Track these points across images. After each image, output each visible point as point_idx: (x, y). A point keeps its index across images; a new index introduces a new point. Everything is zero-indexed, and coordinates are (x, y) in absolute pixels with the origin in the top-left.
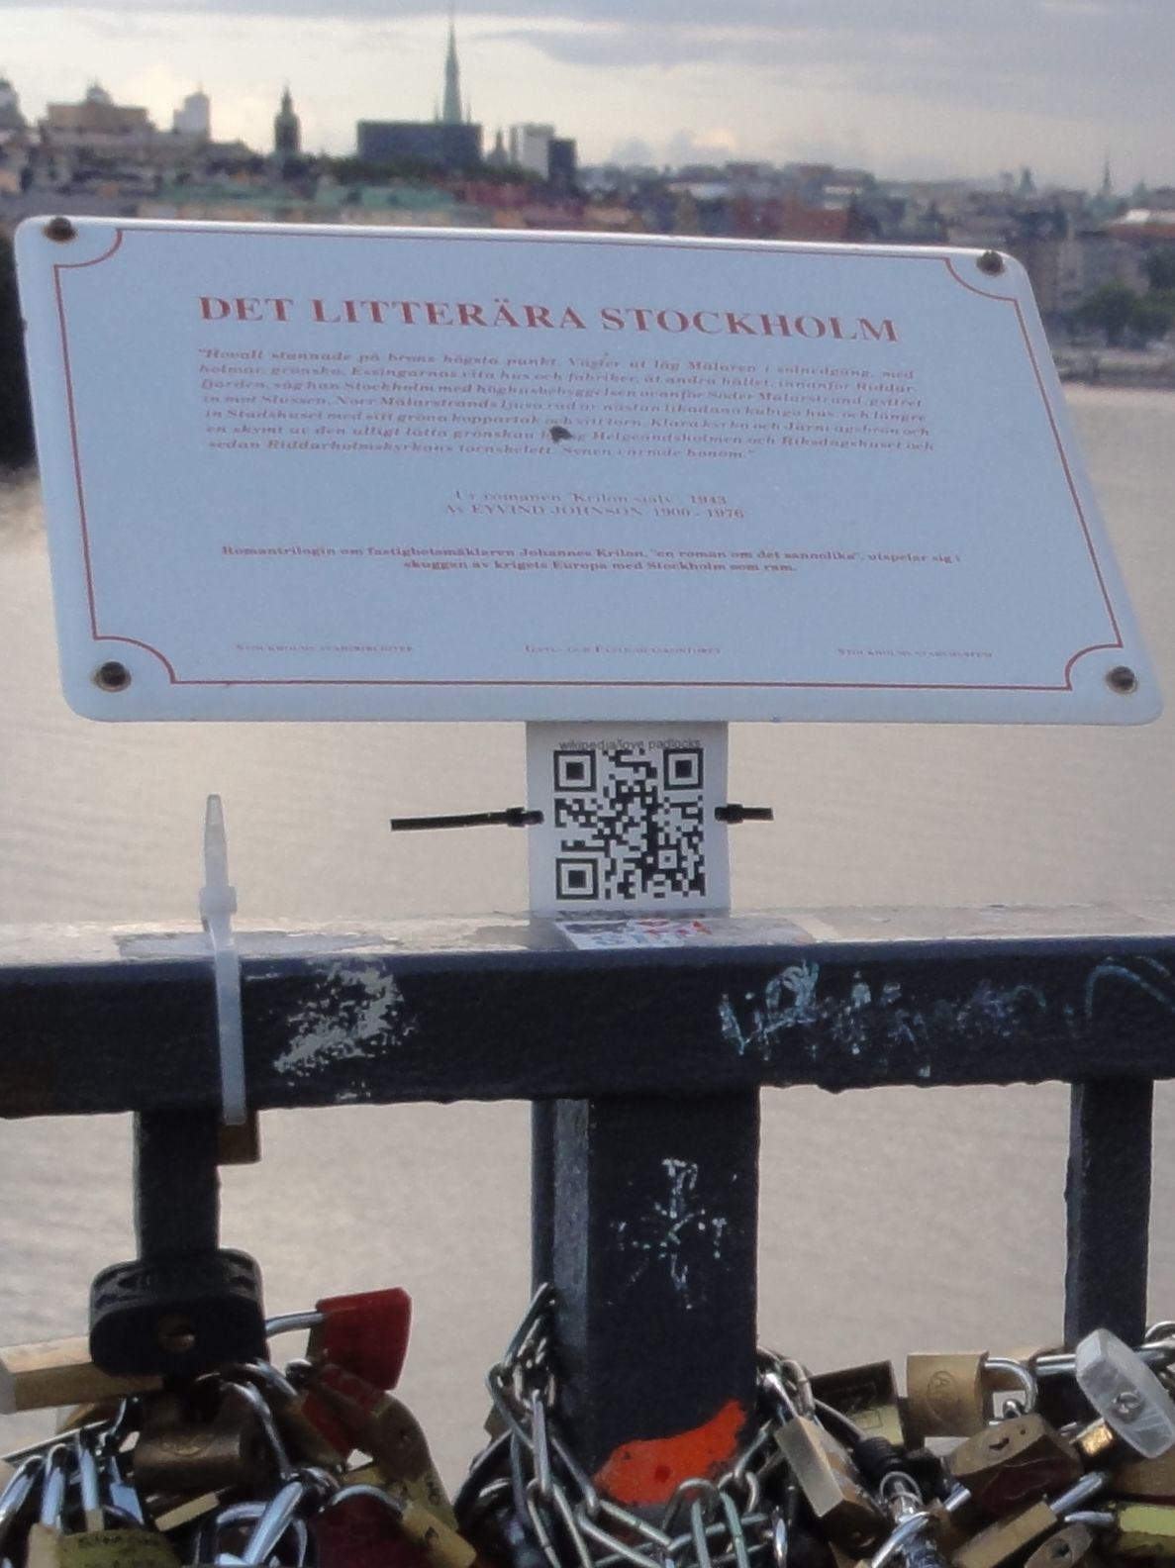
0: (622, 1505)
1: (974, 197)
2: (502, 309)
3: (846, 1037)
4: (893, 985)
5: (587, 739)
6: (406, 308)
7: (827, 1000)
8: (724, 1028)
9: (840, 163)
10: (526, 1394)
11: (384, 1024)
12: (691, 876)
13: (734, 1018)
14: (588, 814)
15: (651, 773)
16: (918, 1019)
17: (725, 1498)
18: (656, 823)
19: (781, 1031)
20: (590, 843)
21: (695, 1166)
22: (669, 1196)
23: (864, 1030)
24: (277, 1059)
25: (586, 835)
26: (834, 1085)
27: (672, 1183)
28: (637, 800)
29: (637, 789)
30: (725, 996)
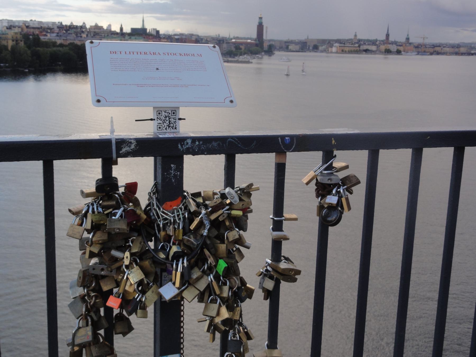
0: (166, 210)
1: (212, 38)
2: (150, 53)
5: (161, 109)
8: (179, 147)
9: (194, 33)
10: (153, 196)
11: (134, 147)
12: (175, 127)
14: (161, 119)
15: (169, 114)
16: (205, 146)
17: (179, 209)
19: (186, 148)
20: (161, 123)
25: (161, 122)
28: (168, 117)
29: (168, 116)
30: (179, 143)
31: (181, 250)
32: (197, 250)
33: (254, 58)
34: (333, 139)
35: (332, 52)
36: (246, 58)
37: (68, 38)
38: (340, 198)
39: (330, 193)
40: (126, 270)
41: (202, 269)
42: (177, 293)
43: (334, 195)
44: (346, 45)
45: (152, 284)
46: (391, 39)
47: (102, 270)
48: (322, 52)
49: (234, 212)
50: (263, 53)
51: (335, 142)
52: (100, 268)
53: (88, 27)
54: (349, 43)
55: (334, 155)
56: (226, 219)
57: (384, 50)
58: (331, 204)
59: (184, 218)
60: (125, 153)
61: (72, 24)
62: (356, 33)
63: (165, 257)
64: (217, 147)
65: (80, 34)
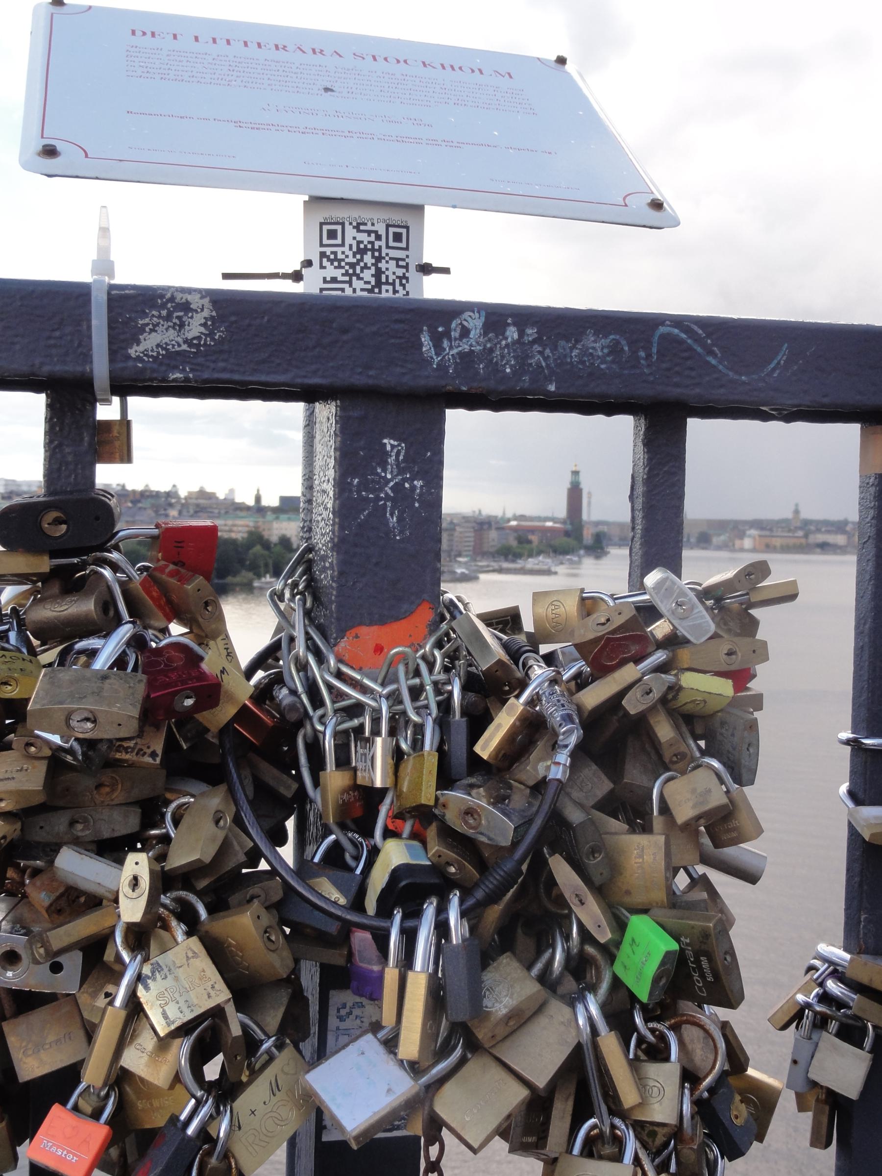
0: (352, 668)
3: (502, 361)
4: (532, 329)
7: (490, 335)
8: (424, 349)
11: (202, 329)
13: (430, 343)
15: (378, 237)
16: (548, 352)
18: (381, 268)
19: (459, 353)
20: (340, 278)
21: (403, 445)
22: (386, 463)
23: (513, 357)
24: (131, 348)
25: (338, 274)
27: (387, 454)
28: (369, 253)
29: (369, 246)
30: (425, 328)
31: (429, 863)
33: (562, 563)
35: (742, 550)
36: (543, 562)
37: (137, 518)
40: (126, 956)
42: (404, 1098)
44: (775, 534)
48: (719, 548)
50: (582, 552)
53: (183, 493)
54: (782, 528)
56: (652, 709)
59: (445, 706)
60: (155, 358)
61: (147, 488)
62: (797, 505)
64: (609, 359)
65: (165, 510)
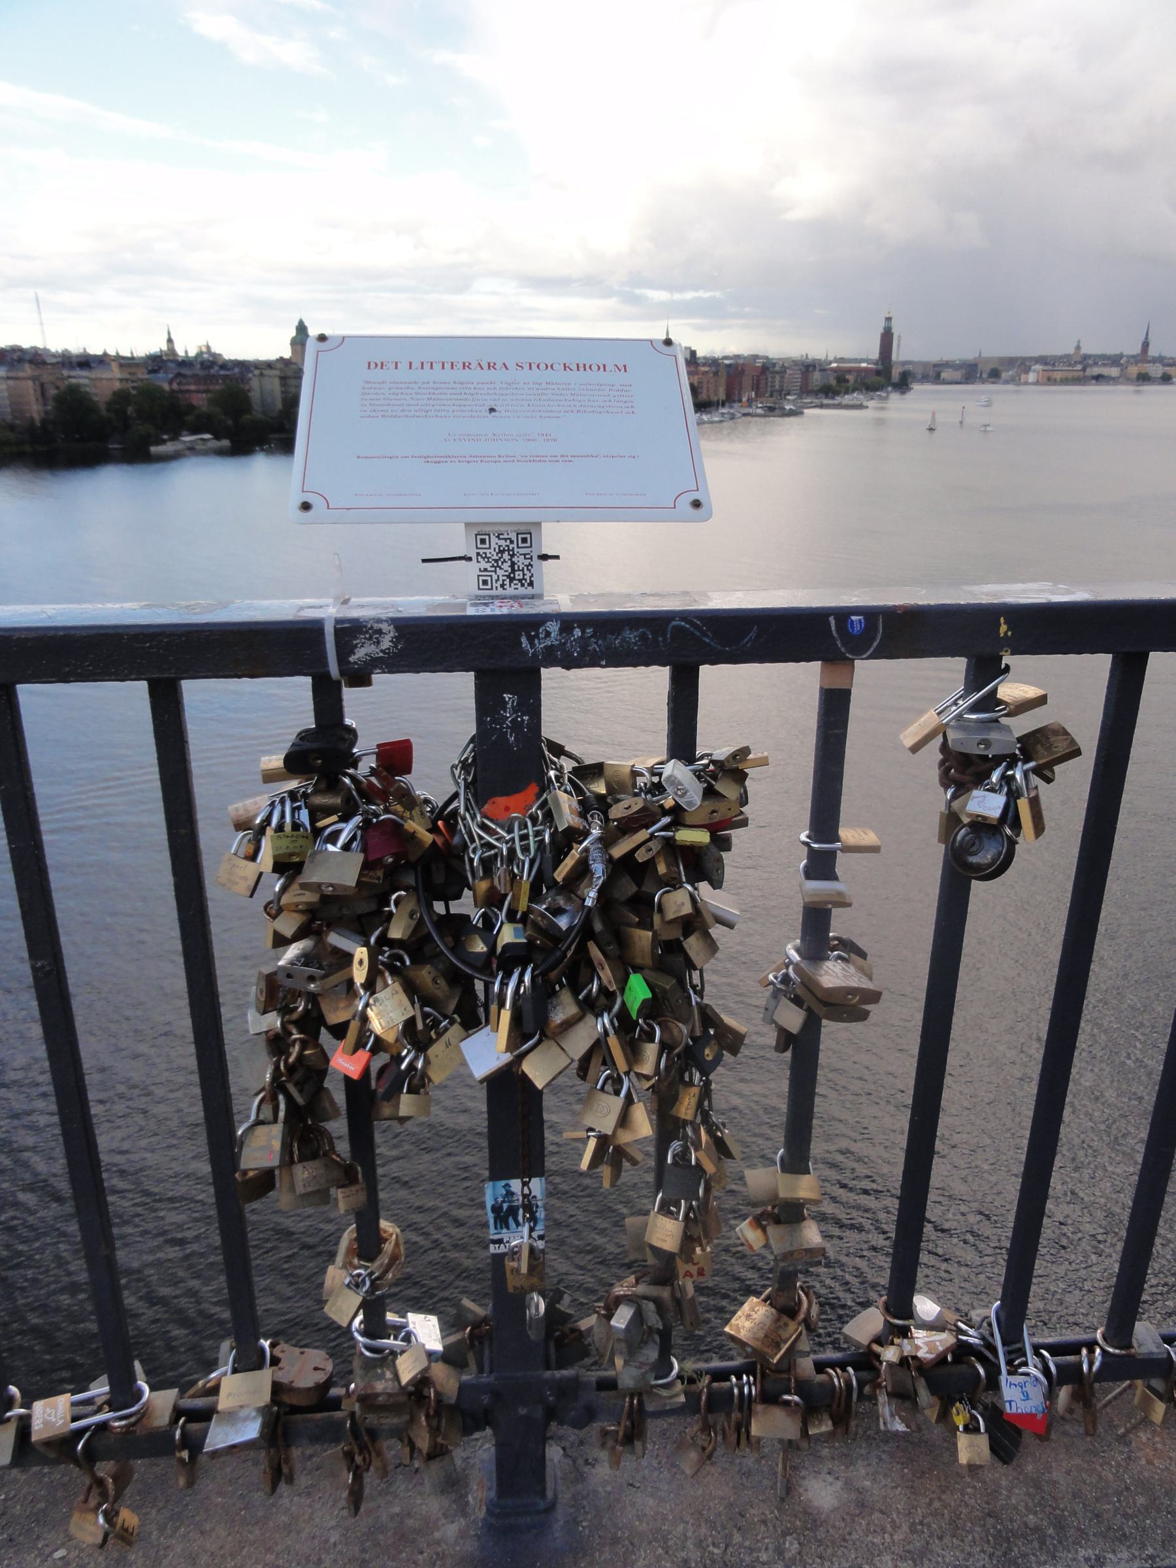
1: (793, 361)
5: (487, 529)
6: (443, 364)
9: (761, 354)
14: (488, 558)
15: (512, 542)
16: (600, 642)
17: (528, 820)
19: (545, 647)
20: (489, 569)
25: (488, 566)
26: (568, 668)
27: (507, 703)
31: (525, 941)
32: (563, 949)
33: (872, 399)
34: (1002, 620)
35: (1026, 383)
38: (1012, 800)
39: (980, 779)
41: (585, 991)
43: (992, 790)
45: (449, 1023)
46: (1153, 352)
47: (312, 979)
48: (1007, 382)
49: (686, 836)
51: (1008, 629)
52: (306, 975)
55: (1003, 666)
57: (1135, 376)
58: (984, 818)
63: (485, 949)
